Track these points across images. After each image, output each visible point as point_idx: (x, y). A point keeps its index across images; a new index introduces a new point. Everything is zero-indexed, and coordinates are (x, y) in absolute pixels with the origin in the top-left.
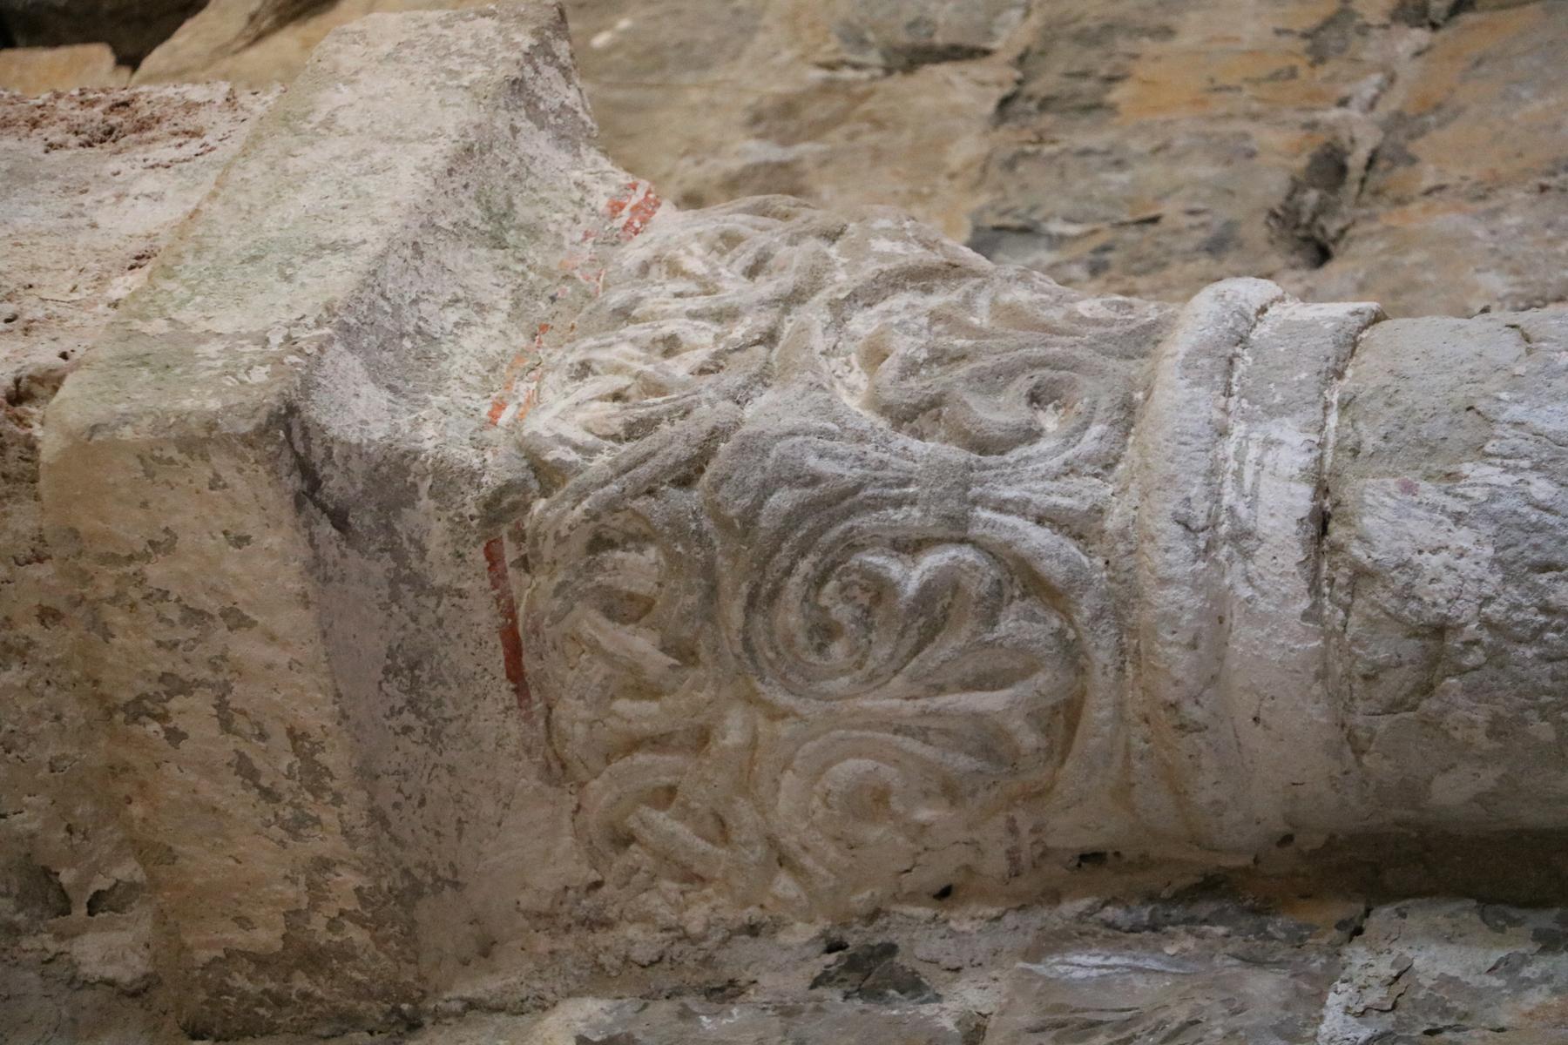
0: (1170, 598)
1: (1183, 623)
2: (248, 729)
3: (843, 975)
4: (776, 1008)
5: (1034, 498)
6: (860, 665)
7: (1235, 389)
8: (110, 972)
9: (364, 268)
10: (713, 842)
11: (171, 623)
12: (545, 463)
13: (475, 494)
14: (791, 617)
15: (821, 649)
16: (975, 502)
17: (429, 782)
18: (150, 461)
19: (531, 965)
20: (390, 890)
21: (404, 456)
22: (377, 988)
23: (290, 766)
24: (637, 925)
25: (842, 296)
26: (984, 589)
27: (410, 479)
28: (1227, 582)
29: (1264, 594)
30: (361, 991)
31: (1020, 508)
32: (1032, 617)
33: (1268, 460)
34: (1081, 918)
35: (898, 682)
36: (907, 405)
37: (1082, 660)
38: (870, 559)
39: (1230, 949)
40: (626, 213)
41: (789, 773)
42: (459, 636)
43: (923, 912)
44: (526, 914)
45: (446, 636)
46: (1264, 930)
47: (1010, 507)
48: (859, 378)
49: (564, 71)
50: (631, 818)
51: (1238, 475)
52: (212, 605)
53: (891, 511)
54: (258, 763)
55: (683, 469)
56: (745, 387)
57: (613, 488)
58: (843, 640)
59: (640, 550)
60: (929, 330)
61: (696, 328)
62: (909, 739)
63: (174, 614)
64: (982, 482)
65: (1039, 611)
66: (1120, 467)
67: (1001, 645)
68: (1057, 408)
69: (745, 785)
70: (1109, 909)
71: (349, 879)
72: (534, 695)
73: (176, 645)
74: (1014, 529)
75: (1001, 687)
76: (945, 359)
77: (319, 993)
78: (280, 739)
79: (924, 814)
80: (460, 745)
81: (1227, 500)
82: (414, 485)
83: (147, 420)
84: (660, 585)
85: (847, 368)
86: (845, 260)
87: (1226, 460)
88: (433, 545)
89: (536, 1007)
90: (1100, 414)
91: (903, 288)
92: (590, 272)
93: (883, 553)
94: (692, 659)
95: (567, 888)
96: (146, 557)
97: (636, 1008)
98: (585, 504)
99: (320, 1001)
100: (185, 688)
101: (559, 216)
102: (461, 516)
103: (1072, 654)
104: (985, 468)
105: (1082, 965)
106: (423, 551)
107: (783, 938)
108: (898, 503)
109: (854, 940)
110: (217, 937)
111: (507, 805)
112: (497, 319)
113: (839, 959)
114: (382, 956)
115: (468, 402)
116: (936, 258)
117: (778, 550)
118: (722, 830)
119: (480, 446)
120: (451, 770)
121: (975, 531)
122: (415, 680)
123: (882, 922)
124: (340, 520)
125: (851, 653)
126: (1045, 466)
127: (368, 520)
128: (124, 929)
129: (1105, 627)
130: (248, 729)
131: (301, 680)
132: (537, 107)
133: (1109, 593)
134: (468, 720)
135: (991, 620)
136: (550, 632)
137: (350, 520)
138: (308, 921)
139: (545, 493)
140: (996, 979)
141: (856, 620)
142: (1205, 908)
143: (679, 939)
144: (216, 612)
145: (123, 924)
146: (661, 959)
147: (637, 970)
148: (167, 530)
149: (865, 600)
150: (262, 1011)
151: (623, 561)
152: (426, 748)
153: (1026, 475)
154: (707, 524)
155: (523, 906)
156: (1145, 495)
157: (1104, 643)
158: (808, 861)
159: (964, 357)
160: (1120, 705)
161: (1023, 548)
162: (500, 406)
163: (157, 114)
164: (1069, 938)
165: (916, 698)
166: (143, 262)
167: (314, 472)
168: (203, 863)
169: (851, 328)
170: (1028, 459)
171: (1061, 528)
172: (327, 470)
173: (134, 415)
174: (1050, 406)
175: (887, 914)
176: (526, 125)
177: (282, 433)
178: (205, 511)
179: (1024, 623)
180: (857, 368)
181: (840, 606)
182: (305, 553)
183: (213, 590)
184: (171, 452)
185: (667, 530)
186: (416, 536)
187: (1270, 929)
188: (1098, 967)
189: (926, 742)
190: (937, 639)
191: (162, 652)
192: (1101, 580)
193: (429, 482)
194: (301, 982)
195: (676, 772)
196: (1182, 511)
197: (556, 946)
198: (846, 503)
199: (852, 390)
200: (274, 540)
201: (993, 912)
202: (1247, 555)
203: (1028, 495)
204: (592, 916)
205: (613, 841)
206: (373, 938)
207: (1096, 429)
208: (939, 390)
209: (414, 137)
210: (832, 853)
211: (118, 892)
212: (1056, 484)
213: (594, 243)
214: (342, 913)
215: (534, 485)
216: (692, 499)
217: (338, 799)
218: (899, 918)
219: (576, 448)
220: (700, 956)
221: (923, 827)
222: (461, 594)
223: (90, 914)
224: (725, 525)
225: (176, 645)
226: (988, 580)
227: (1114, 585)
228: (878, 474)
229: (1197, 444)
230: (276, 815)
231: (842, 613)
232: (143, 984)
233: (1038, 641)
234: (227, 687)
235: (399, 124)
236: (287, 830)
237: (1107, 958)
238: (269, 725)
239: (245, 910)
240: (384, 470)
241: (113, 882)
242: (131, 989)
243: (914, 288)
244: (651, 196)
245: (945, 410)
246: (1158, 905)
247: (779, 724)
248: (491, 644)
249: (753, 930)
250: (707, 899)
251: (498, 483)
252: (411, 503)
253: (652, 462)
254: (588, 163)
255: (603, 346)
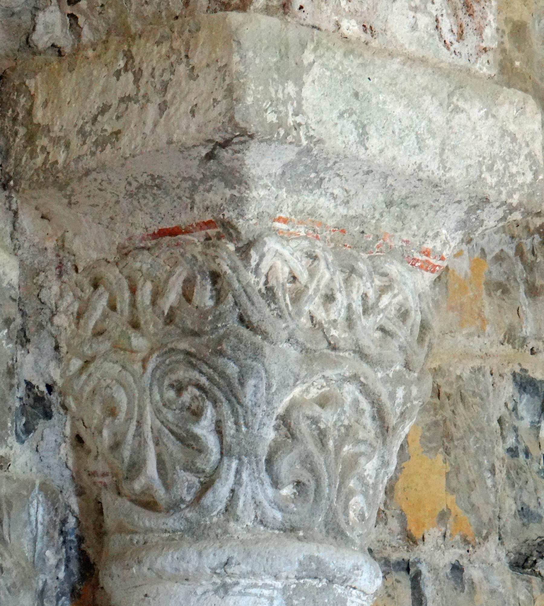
0: (192, 557)
1: (182, 563)
2: (120, 110)
3: (32, 396)
4: (13, 365)
5: (243, 488)
6: (164, 405)
7: (302, 581)
8: (40, 28)
9: (348, 153)
10: (94, 328)
11: (161, 76)
12: (250, 250)
13: (234, 217)
14: (183, 374)
15: (171, 386)
16: (240, 459)
17: (111, 193)
18: (224, 69)
19: (37, 240)
20: (58, 177)
21: (246, 183)
22: (19, 169)
23: (106, 130)
24: (58, 290)
25: (362, 379)
26: (198, 465)
27: (237, 186)
28: (204, 582)
29: (198, 600)
30: (18, 160)
31: (238, 482)
32: (189, 488)
33: (263, 599)
34: (68, 506)
35: (158, 423)
36: (290, 423)
37: (172, 511)
38: (209, 411)
39: (49, 582)
40: (424, 258)
41: (120, 369)
42: (175, 207)
43: (68, 431)
44: (63, 236)
45: (174, 201)
46: (63, 595)
47: (238, 476)
48: (314, 392)
49: (504, 218)
50: (103, 288)
51: (255, 586)
52: (169, 97)
53: (232, 420)
54: (107, 115)
55: (247, 319)
56: (297, 342)
57: (236, 285)
58: (175, 397)
59: (211, 297)
60: (341, 426)
61: (340, 310)
62: (135, 428)
63: (166, 77)
64: (250, 462)
65: (194, 490)
66: (262, 528)
67: (174, 474)
68: (295, 494)
69: (116, 347)
70: (74, 520)
71: (61, 158)
72: (154, 242)
73: (153, 77)
74: (227, 479)
75: (159, 472)
76: (322, 437)
77: (17, 140)
78: (118, 126)
79: (105, 433)
80: (130, 206)
81: (243, 582)
82: (235, 188)
83: (241, 68)
84: (197, 307)
85: (319, 387)
86: (391, 375)
87: (262, 579)
88: (211, 195)
89: (15, 245)
90: (288, 516)
91: (373, 407)
92: (383, 248)
93: (213, 417)
94: (168, 321)
95: (74, 255)
96: (188, 64)
97: (13, 296)
98: (229, 271)
99: (14, 141)
100: (137, 81)
101: (415, 227)
102: (224, 210)
103: (174, 507)
104: (257, 463)
105: (38, 512)
106: (208, 191)
107: (53, 364)
108: (236, 423)
109: (54, 397)
110: (39, 91)
111: (107, 227)
112: (342, 210)
113: (42, 392)
114: (32, 172)
115: (286, 207)
116: (392, 421)
117: (210, 367)
118: (98, 333)
119: (260, 216)
120: (117, 202)
121: (226, 460)
122: (152, 187)
123: (62, 411)
124: (210, 156)
125: (169, 401)
126: (256, 494)
127: (214, 168)
128: (62, 31)
129: (183, 524)
130: (120, 110)
131: (139, 139)
132: (478, 209)
133: (199, 525)
134: (141, 210)
135: (186, 469)
136: (178, 251)
137: (212, 161)
138: (45, 136)
139: (238, 250)
140: (31, 470)
141: (183, 403)
142: (74, 567)
143: (52, 312)
144: (165, 98)
145: (64, 31)
146: (43, 303)
147: (35, 294)
148: (198, 76)
149: (194, 407)
150: (10, 111)
151: (206, 289)
152: (124, 192)
153: (254, 483)
154: (221, 331)
155: (67, 234)
156: (243, 542)
157: (176, 524)
158: (84, 377)
159: (323, 445)
160: (152, 531)
161: (217, 484)
162: (285, 221)
163: (475, 14)
164: (53, 504)
165: (152, 432)
166: (369, 31)
167: (227, 146)
168: (68, 84)
169: (345, 385)
170: (262, 484)
171: (230, 501)
172: (230, 151)
173: (245, 61)
174: (295, 491)
175: (66, 414)
176: (465, 206)
177: (238, 134)
178: (205, 95)
179: (186, 484)
180: (320, 391)
181: (189, 396)
182: (190, 143)
183: (174, 97)
184: (227, 82)
185: (217, 312)
186: (213, 188)
187: (63, 598)
188: (36, 520)
189: (134, 436)
190: (178, 442)
191: (150, 70)
192: (205, 521)
193: (238, 195)
194: (22, 131)
195: (122, 311)
196: (234, 561)
197: (49, 251)
198: (233, 399)
199: (307, 390)
200: (193, 129)
201: (70, 464)
202: (216, 592)
203: (244, 484)
204: (64, 268)
205: (95, 278)
206: (39, 168)
207: (279, 516)
208: (300, 438)
209: (444, 157)
210: (88, 389)
211: (78, 28)
212: (250, 498)
213: (402, 246)
214: (48, 153)
215: (240, 245)
216: (232, 322)
217: (93, 154)
218: (64, 419)
219: (258, 265)
220: (44, 323)
221: (100, 432)
222: (192, 208)
223: (68, 15)
224: (219, 342)
225: (153, 77)
226: (204, 467)
227: (202, 528)
228: (249, 413)
229: (268, 567)
230: (87, 123)
231: (186, 397)
232: (32, 45)
233: (177, 491)
234: (137, 102)
235: (454, 147)
236: (81, 128)
237: (42, 524)
238: (122, 121)
239: (50, 104)
240: (238, 175)
241: (81, 26)
242: (29, 40)
243: (373, 412)
244: (437, 268)
245: (290, 441)
246: (76, 544)
247: (140, 364)
248: (173, 222)
249: (57, 348)
250: (70, 326)
251: (240, 227)
252: (226, 186)
253: (249, 304)
254: (453, 235)
255: (327, 265)
